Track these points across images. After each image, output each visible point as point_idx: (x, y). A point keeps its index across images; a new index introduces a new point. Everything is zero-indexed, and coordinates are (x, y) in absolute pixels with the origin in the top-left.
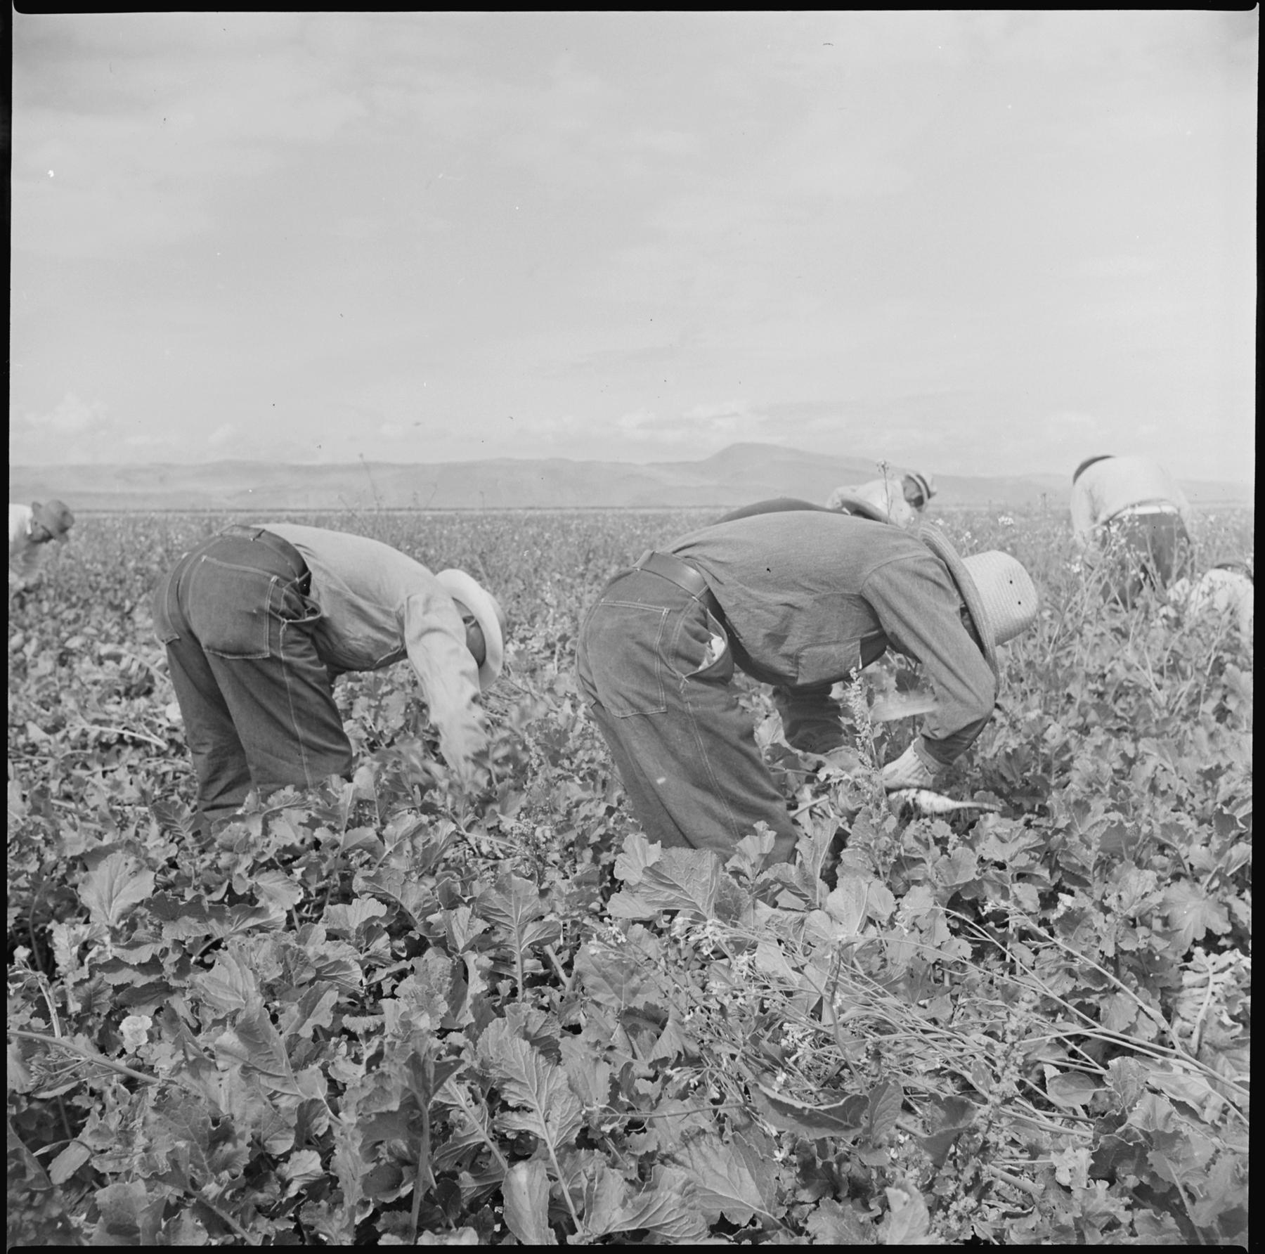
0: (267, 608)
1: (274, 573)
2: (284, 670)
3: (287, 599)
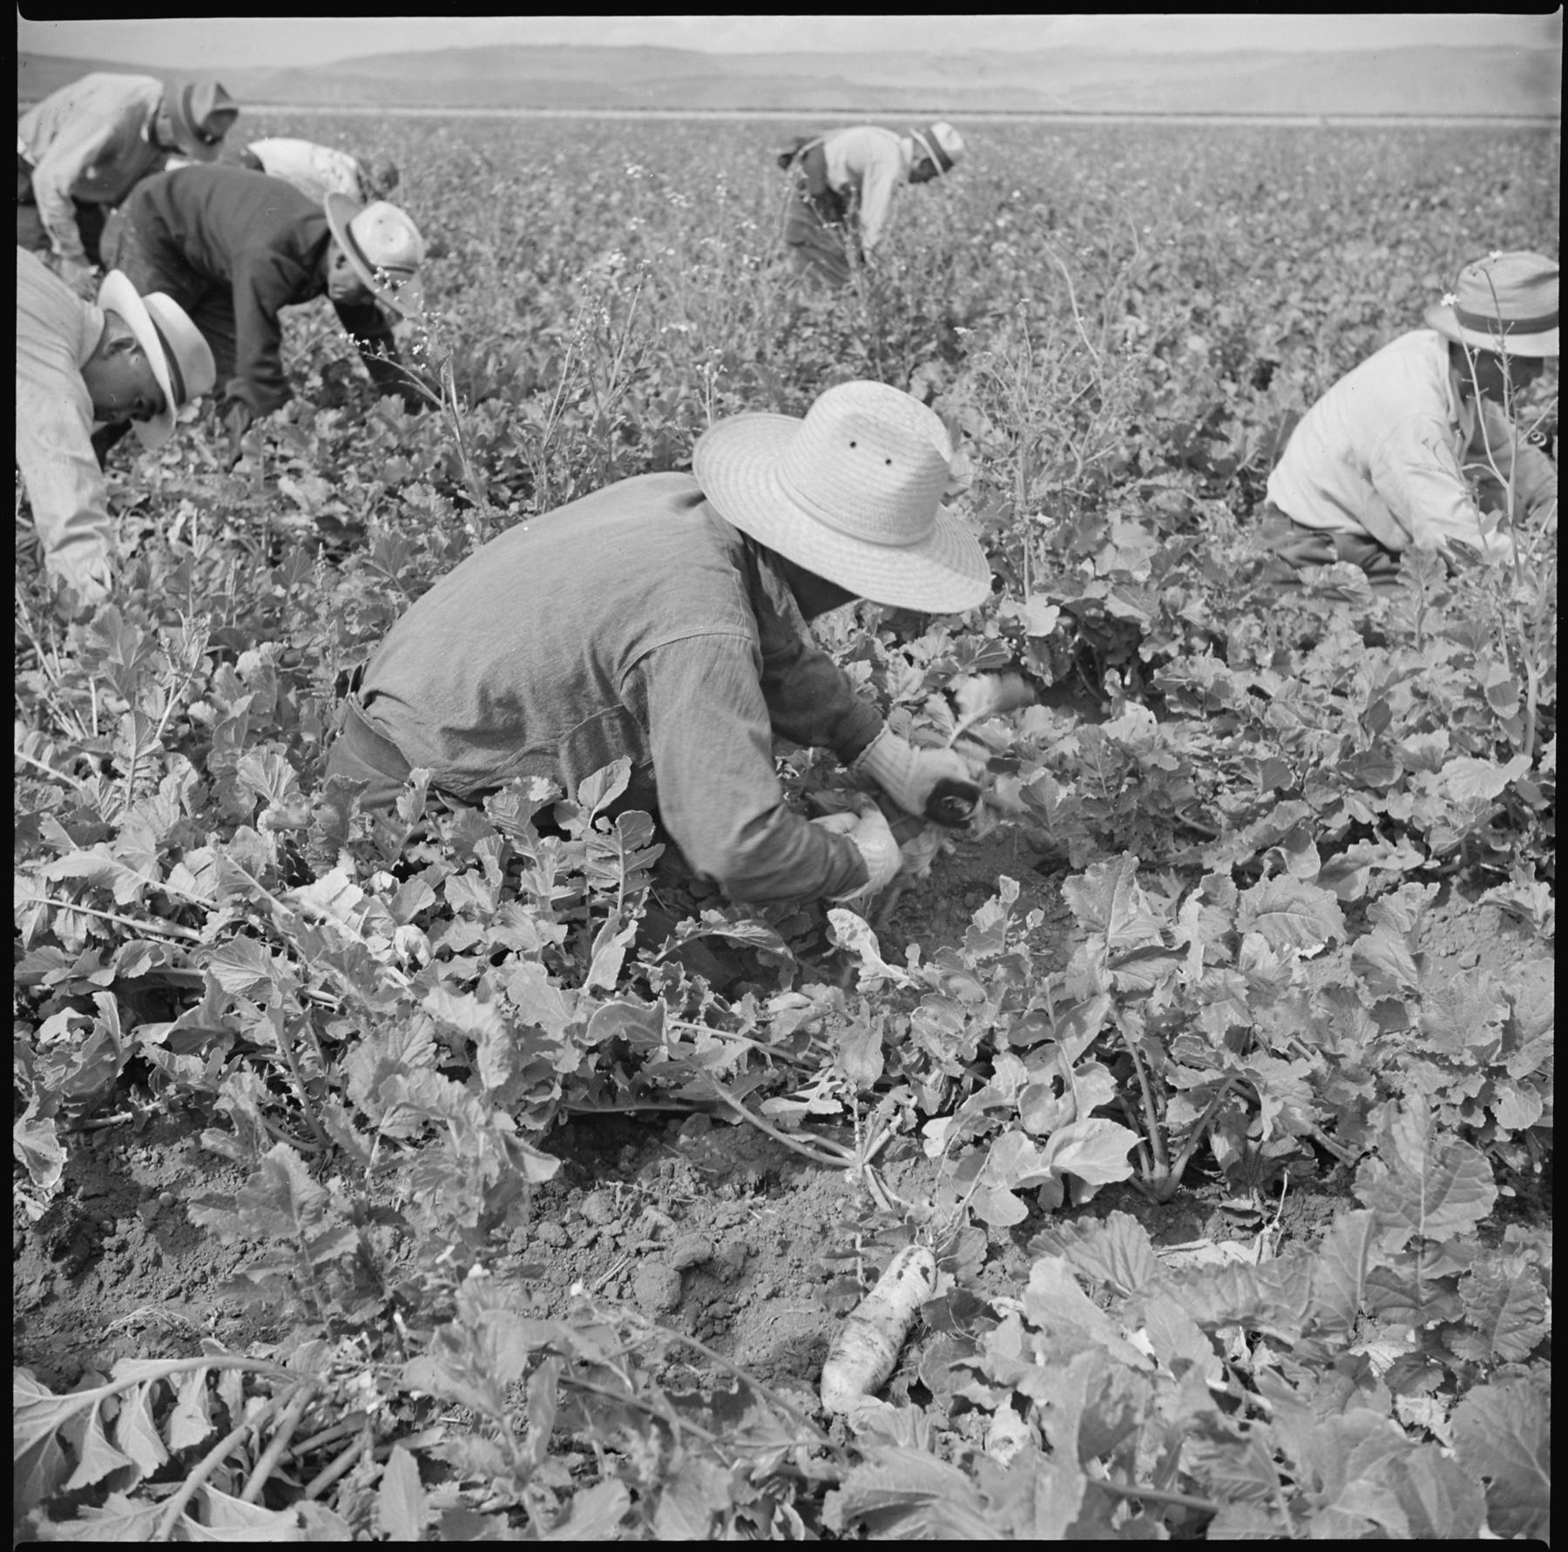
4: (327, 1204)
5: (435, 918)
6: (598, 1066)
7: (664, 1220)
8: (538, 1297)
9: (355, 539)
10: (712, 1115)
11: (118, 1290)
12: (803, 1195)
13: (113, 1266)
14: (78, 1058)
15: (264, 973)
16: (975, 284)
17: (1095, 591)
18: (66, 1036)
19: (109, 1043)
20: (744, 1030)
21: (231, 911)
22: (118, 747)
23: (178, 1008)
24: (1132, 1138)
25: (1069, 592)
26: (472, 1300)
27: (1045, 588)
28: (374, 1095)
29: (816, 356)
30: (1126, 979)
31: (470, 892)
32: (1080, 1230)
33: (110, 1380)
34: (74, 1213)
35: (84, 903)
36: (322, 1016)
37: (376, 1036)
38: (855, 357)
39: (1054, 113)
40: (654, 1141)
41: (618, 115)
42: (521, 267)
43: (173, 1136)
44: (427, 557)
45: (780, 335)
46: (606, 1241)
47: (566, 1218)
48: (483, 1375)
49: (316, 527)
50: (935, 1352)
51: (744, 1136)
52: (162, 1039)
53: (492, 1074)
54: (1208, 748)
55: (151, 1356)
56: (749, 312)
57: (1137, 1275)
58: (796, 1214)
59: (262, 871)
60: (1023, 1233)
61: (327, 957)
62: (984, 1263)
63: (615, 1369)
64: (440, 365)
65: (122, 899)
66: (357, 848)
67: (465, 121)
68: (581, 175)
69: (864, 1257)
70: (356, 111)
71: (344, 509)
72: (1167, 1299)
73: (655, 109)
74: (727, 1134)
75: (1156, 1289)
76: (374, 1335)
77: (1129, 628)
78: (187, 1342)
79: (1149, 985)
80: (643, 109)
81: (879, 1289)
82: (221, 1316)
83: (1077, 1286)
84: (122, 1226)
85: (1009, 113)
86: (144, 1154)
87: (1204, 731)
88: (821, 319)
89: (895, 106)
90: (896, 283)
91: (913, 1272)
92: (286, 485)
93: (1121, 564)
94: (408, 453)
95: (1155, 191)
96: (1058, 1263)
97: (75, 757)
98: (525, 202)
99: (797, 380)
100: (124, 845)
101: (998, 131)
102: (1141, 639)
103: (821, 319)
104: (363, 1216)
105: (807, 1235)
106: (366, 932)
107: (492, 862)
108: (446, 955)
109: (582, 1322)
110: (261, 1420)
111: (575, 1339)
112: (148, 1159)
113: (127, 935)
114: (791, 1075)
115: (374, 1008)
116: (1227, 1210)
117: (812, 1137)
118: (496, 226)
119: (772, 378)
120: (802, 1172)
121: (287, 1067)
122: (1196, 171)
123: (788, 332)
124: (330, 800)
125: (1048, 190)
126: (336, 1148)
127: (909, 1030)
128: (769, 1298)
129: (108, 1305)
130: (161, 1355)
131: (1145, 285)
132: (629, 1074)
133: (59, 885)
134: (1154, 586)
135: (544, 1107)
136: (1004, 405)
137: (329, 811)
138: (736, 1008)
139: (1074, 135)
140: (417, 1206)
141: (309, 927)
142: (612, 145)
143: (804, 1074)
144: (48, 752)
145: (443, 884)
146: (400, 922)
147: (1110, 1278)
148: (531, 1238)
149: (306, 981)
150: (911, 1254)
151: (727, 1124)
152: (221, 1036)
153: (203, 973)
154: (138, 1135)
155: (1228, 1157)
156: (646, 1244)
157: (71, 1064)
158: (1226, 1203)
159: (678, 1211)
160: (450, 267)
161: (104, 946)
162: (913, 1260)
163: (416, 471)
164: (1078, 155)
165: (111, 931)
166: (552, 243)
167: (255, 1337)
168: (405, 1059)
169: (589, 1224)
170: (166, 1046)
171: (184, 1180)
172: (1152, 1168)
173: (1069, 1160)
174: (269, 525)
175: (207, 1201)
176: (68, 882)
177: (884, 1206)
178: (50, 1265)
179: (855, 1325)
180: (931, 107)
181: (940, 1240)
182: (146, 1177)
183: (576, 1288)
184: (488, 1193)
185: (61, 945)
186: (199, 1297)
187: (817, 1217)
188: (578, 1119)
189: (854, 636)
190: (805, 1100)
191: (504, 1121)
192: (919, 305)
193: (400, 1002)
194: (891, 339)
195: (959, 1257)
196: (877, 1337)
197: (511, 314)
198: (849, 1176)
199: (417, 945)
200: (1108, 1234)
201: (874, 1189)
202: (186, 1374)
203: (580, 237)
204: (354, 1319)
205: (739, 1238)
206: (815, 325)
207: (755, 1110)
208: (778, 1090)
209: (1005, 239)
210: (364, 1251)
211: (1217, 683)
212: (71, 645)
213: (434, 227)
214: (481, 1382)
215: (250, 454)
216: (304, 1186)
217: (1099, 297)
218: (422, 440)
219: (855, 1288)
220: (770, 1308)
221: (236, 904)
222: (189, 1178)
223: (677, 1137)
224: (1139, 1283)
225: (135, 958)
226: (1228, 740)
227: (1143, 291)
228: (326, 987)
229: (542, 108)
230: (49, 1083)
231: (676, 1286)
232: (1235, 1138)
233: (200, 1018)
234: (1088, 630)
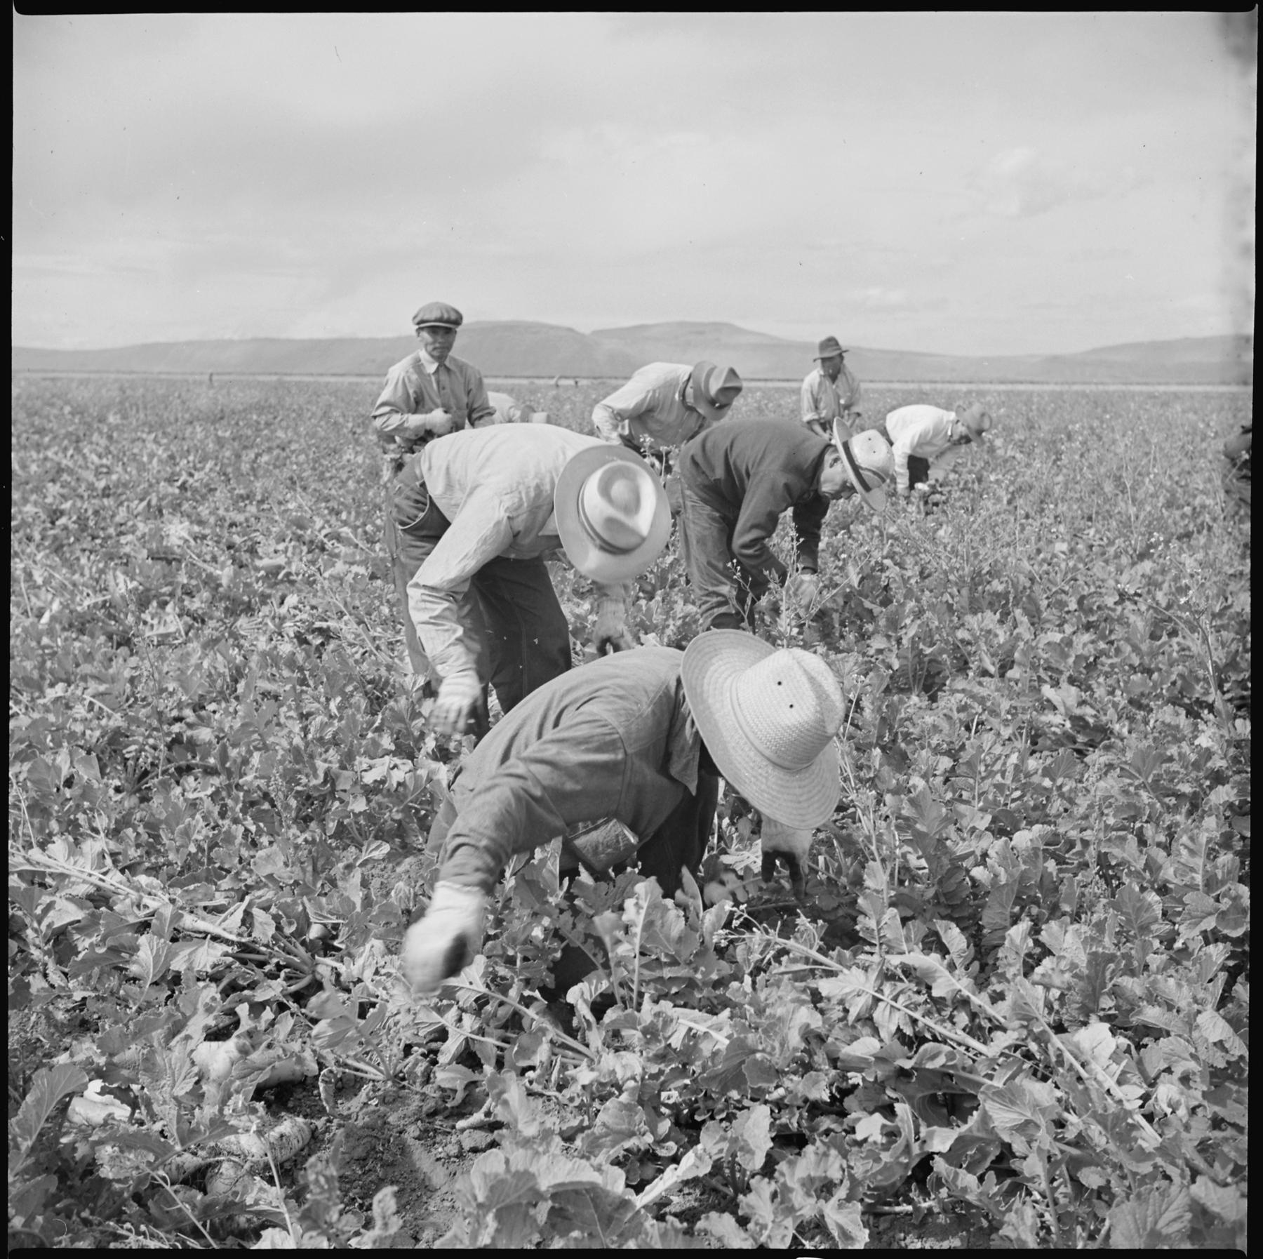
9: (1098, 737)
44: (1175, 767)
49: (1068, 725)
67: (1192, 396)
70: (1101, 388)
71: (1094, 712)
92: (1047, 691)
94: (1149, 672)
115: (1130, 1166)
154: (915, 1227)
157: (878, 1160)
160: (1183, 516)
163: (1155, 687)
174: (1030, 722)
215: (1020, 664)
218: (1162, 661)
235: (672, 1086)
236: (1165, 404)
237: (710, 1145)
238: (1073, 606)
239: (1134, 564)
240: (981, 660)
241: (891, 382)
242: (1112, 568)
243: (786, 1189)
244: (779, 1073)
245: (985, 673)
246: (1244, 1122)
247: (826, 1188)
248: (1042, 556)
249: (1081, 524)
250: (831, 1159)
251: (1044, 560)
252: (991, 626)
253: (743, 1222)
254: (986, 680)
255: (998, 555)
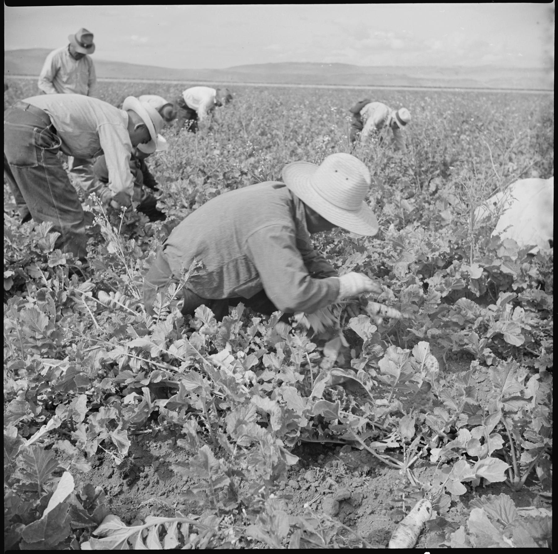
0: (34, 143)
1: (35, 126)
2: (46, 172)
3: (42, 138)
4: (219, 468)
5: (260, 368)
6: (313, 425)
7: (334, 483)
8: (290, 506)
10: (353, 446)
11: (144, 491)
12: (384, 477)
13: (143, 483)
14: (136, 410)
15: (200, 384)
16: (454, 150)
17: (496, 263)
18: (133, 402)
19: (147, 406)
20: (365, 416)
21: (189, 362)
22: (155, 304)
23: (169, 394)
24: (506, 466)
25: (487, 263)
26: (271, 506)
27: (478, 261)
28: (235, 431)
29: (396, 174)
30: (508, 407)
31: (270, 360)
32: (489, 499)
33: (144, 523)
34: (131, 463)
35: (140, 356)
36: (218, 400)
37: (237, 410)
38: (409, 175)
39: (483, 89)
40: (330, 453)
41: (326, 87)
42: (292, 140)
43: (165, 439)
45: (383, 166)
46: (313, 489)
47: (299, 479)
48: (274, 534)
50: (431, 539)
51: (363, 454)
52: (165, 404)
53: (276, 426)
54: (538, 323)
55: (155, 515)
56: (372, 158)
57: (510, 518)
58: (381, 484)
59: (200, 348)
60: (465, 498)
61: (221, 381)
62: (450, 508)
63: (319, 535)
64: (267, 175)
65: (153, 355)
66: (233, 342)
67: (273, 88)
68: (313, 108)
69: (405, 502)
70: (235, 84)
72: (521, 528)
73: (339, 85)
74: (357, 453)
75: (517, 524)
76: (234, 515)
77: (509, 277)
78: (168, 512)
79: (516, 410)
80: (335, 85)
81: (411, 514)
82: (178, 503)
83: (489, 520)
84: (147, 469)
85: (466, 88)
86: (155, 445)
87: (537, 317)
88: (398, 161)
89: (425, 85)
90: (426, 149)
91: (423, 509)
93: (507, 254)
95: (521, 118)
96: (481, 511)
97: (136, 305)
98: (293, 117)
99: (389, 182)
100: (155, 337)
101: (463, 95)
102: (513, 282)
103: (398, 161)
104: (231, 473)
105: (385, 492)
106: (234, 372)
107: (280, 350)
108: (261, 382)
109: (307, 517)
110: (195, 542)
111: (305, 523)
112: (156, 446)
113: (154, 368)
114: (381, 433)
115: (237, 399)
116: (542, 496)
117: (388, 457)
118: (283, 125)
119: (380, 182)
120: (384, 469)
121: (205, 418)
122: (536, 111)
123: (386, 165)
124: (224, 325)
125: (481, 117)
126: (220, 447)
127: (425, 420)
128: (370, 514)
129: (141, 496)
130: (158, 515)
131: (516, 152)
132: (323, 429)
133: (132, 349)
134: (519, 262)
135: (293, 439)
136: (465, 194)
137: (224, 329)
138: (362, 408)
139: (491, 97)
140: (249, 471)
141: (215, 369)
142: (325, 98)
143: (386, 433)
144: (128, 303)
145: (262, 357)
146: (246, 369)
147: (499, 518)
148: (286, 485)
149: (213, 388)
150: (423, 502)
151: (358, 450)
152: (183, 405)
153: (179, 383)
154: (153, 438)
155: (543, 476)
156: (327, 491)
157: (134, 412)
158: (541, 493)
159: (339, 480)
160: (268, 139)
161: (146, 371)
162: (424, 504)
164: (492, 104)
165: (148, 366)
166: (303, 132)
167: (190, 512)
168: (246, 419)
169: (307, 482)
170: (165, 407)
171: (168, 455)
172: (514, 478)
173: (482, 472)
175: (178, 464)
176: (136, 349)
177: (413, 484)
178: (122, 480)
179: (402, 527)
180: (438, 85)
181: (433, 498)
182: (155, 452)
183: (306, 505)
184: (274, 468)
185: (131, 370)
186: (171, 495)
187: (389, 486)
188: (304, 444)
189: (408, 276)
190: (386, 443)
191: (280, 443)
192: (434, 157)
193: (246, 398)
194: (423, 169)
195: (440, 505)
196: (409, 532)
197: (288, 157)
198: (401, 472)
199: (253, 378)
200: (499, 502)
201: (410, 477)
202: (171, 523)
203: (312, 130)
204: (227, 509)
205: (360, 491)
206: (395, 163)
207: (368, 445)
208: (376, 439)
209: (465, 134)
210: (232, 485)
211: (542, 300)
212: (137, 267)
213: (262, 125)
214: (272, 535)
216: (213, 461)
217: (499, 155)
219: (402, 512)
220: (371, 517)
221: (191, 359)
222: (170, 454)
223: (339, 453)
224: (511, 521)
225: (156, 376)
226: (545, 321)
227: (515, 154)
228: (220, 391)
229: (300, 84)
230: (126, 418)
231: (337, 507)
232: (545, 469)
233: (177, 398)
234: (493, 277)
235: (43, 391)
236: (261, 92)
237: (61, 414)
238: (221, 177)
239: (247, 159)
240: (181, 201)
241: (143, 79)
242: (237, 161)
243: (92, 426)
244: (91, 380)
245: (183, 207)
246: (5, 214)
247: (112, 424)
248: (208, 156)
249: (226, 142)
250: (111, 411)
251: (209, 158)
252: (185, 186)
253: (74, 442)
254: (184, 210)
255: (189, 155)
